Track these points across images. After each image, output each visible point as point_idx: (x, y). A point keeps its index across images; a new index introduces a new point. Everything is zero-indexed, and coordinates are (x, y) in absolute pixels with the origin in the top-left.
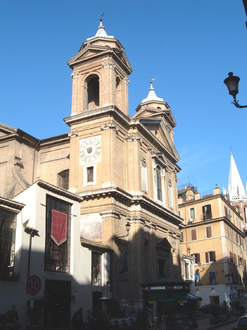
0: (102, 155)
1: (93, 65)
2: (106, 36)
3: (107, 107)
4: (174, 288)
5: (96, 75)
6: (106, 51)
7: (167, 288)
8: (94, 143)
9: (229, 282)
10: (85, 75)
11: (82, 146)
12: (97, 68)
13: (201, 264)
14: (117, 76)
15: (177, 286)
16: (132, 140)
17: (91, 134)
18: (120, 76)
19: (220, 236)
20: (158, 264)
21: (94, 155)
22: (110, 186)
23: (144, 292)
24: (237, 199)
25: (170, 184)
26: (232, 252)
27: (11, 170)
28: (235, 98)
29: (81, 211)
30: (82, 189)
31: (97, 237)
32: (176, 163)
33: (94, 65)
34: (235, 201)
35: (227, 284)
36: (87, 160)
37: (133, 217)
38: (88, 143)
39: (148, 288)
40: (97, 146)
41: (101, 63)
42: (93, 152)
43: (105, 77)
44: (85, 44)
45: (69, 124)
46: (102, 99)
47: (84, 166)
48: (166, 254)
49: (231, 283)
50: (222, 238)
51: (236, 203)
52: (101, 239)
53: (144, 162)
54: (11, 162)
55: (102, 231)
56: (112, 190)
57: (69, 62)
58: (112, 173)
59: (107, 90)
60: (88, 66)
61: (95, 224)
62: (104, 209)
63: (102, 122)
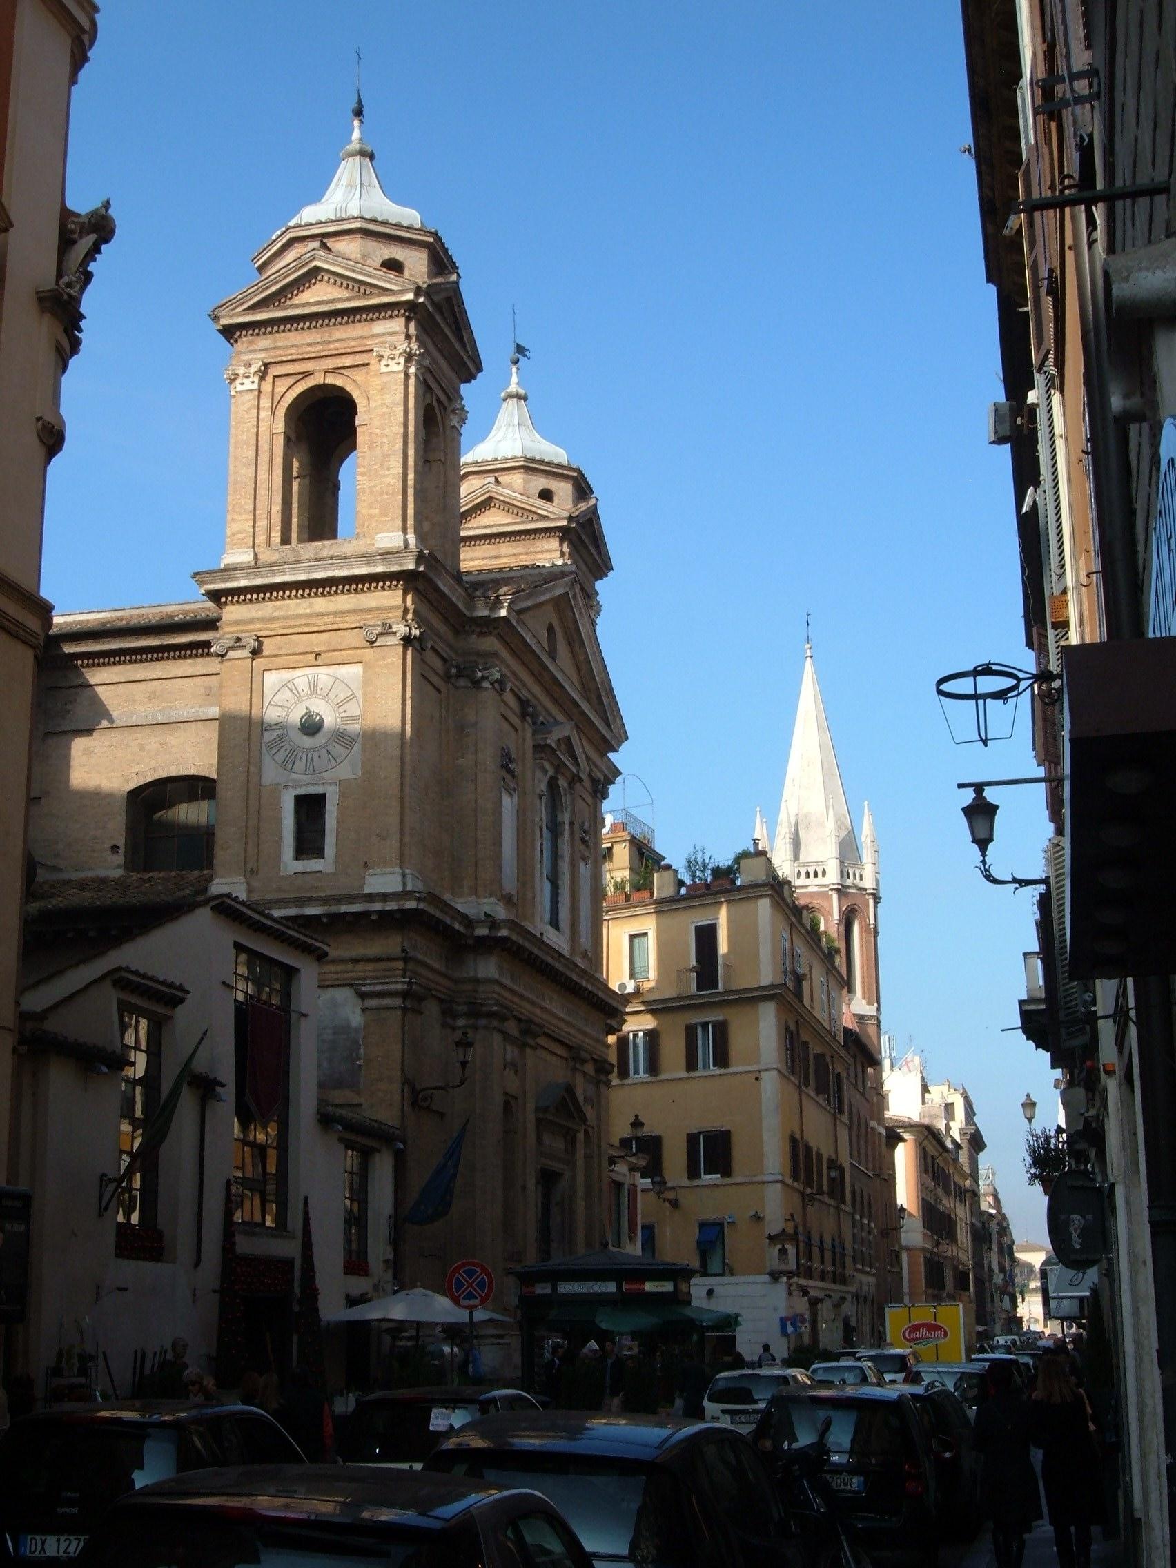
0: (364, 750)
1: (331, 346)
4: (644, 1289)
7: (619, 1287)
8: (332, 695)
9: (783, 1268)
10: (292, 380)
12: (348, 361)
15: (657, 1283)
17: (318, 654)
19: (754, 1068)
21: (330, 748)
24: (816, 875)
26: (798, 1136)
28: (984, 855)
32: (609, 755)
33: (337, 345)
34: (806, 887)
35: (775, 1276)
36: (300, 765)
38: (302, 694)
40: (341, 710)
46: (371, 507)
47: (283, 791)
49: (791, 1272)
50: (763, 1075)
51: (812, 894)
53: (509, 771)
56: (411, 905)
57: (223, 312)
59: (392, 471)
60: (309, 345)
61: (330, 1031)
62: (369, 974)
63: (369, 610)
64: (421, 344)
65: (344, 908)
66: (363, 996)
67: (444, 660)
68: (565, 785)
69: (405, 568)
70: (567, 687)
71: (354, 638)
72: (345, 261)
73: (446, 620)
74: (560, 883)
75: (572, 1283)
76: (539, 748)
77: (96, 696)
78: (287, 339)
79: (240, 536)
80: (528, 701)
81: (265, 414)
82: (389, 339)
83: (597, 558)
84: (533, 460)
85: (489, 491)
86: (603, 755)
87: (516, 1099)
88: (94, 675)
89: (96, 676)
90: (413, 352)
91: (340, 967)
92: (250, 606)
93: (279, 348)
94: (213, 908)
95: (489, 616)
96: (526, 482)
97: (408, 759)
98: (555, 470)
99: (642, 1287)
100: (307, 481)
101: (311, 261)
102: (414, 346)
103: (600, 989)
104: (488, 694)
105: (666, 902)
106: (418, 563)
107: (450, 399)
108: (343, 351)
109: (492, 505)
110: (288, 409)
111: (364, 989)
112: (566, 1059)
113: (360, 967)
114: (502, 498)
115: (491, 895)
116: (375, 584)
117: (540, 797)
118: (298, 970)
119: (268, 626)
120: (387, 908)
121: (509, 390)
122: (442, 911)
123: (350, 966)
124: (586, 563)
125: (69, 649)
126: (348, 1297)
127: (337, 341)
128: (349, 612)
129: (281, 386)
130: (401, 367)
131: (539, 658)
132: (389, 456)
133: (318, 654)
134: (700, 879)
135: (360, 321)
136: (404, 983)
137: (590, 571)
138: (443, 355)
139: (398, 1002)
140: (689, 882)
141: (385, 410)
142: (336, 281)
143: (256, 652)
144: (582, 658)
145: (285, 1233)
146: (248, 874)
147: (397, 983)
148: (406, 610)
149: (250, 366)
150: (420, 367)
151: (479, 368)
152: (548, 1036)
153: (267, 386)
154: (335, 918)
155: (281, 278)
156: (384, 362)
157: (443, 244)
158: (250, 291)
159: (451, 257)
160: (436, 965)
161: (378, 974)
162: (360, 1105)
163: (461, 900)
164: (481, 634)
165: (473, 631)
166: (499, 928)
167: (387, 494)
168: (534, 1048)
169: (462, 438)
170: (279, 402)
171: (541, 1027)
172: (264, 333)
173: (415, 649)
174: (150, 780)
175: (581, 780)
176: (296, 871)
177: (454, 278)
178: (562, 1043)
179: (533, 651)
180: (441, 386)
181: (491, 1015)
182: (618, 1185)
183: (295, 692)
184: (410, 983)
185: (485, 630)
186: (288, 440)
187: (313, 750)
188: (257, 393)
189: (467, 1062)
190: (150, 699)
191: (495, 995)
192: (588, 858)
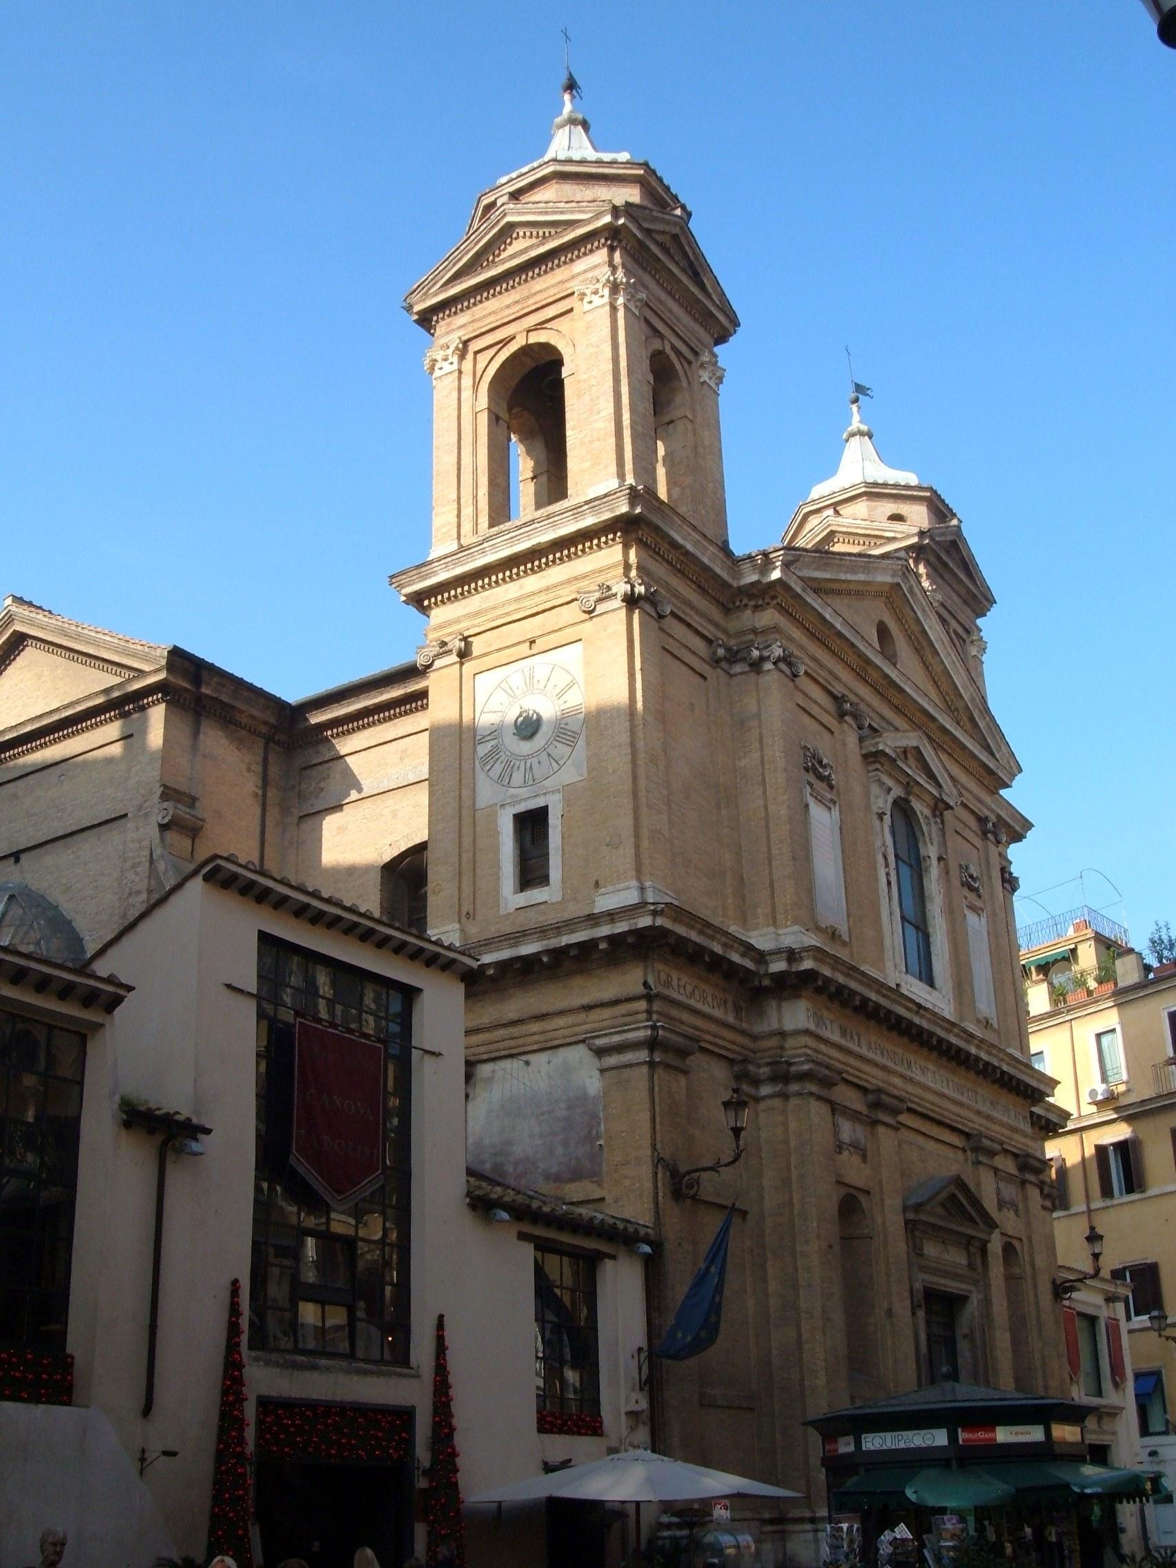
0: (588, 744)
2: (591, 155)
3: (606, 496)
5: (547, 348)
6: (588, 221)
7: (953, 1437)
8: (549, 687)
10: (492, 351)
13: (1166, 1317)
16: (751, 665)
18: (673, 348)
20: (921, 1313)
21: (551, 750)
22: (632, 897)
23: (837, 1467)
25: (972, 897)
27: (147, 853)
29: (469, 1032)
30: (379, 802)
31: (576, 1175)
33: (537, 298)
36: (518, 777)
37: (768, 1064)
38: (517, 692)
39: (851, 1439)
41: (568, 285)
44: (486, 201)
45: (420, 601)
54: (146, 814)
55: (601, 1142)
56: (645, 921)
57: (415, 298)
58: (645, 833)
59: (603, 414)
60: (508, 307)
61: (563, 1105)
64: (628, 273)
65: (565, 940)
66: (600, 1052)
67: (709, 642)
68: (927, 812)
69: (618, 513)
70: (908, 690)
71: (572, 613)
72: (536, 205)
73: (703, 590)
74: (931, 930)
75: (882, 1435)
76: (872, 758)
77: (348, 767)
78: (485, 309)
79: (444, 530)
80: (843, 696)
81: (467, 394)
82: (590, 275)
83: (970, 586)
84: (876, 484)
85: (829, 525)
86: (994, 792)
88: (344, 745)
89: (345, 746)
90: (618, 280)
91: (570, 1019)
92: (456, 604)
93: (478, 320)
94: (207, 878)
95: (758, 582)
96: (870, 510)
97: (640, 744)
98: (904, 492)
99: (991, 1435)
100: (544, 478)
101: (502, 218)
102: (620, 274)
103: (1002, 1060)
104: (771, 678)
105: (1137, 988)
106: (632, 504)
107: (968, 632)
108: (544, 303)
109: (836, 540)
110: (491, 383)
111: (600, 1042)
112: (964, 1150)
113: (595, 1015)
114: (844, 530)
115: (795, 922)
116: (589, 543)
117: (881, 816)
118: (420, 991)
120: (617, 931)
121: (850, 429)
122: (701, 932)
123: (582, 1017)
124: (959, 595)
125: (316, 718)
126: (545, 1464)
127: (535, 294)
128: (562, 583)
129: (483, 359)
130: (606, 299)
131: (853, 645)
132: (598, 398)
133: (532, 642)
134: (1167, 958)
135: (559, 266)
137: (965, 602)
138: (673, 297)
139: (643, 1055)
140: (1156, 964)
141: (591, 350)
142: (531, 233)
143: (464, 655)
144: (939, 669)
145: (406, 1371)
146: (464, 919)
147: (638, 1029)
148: (627, 567)
149: (448, 347)
150: (631, 298)
151: (735, 323)
152: (910, 1110)
153: (468, 365)
154: (559, 954)
155: (472, 245)
156: (586, 299)
157: (939, 496)
158: (441, 268)
159: (947, 506)
160: (717, 1013)
161: (617, 1022)
162: (603, 1199)
163: (755, 933)
164: (757, 608)
165: (746, 605)
166: (801, 959)
167: (599, 440)
168: (896, 1128)
169: (720, 398)
170: (482, 376)
171: (901, 1100)
172: (462, 310)
173: (643, 611)
174: (403, 849)
175: (948, 807)
176: (518, 906)
177: (955, 522)
178: (953, 1129)
179: (840, 635)
180: (677, 334)
181: (804, 1077)
182: (1092, 1320)
183: (510, 692)
184: (654, 1028)
185: (760, 602)
186: (495, 419)
187: (532, 755)
188: (456, 374)
189: (741, 1129)
190: (402, 759)
191: (809, 1051)
192: (982, 910)
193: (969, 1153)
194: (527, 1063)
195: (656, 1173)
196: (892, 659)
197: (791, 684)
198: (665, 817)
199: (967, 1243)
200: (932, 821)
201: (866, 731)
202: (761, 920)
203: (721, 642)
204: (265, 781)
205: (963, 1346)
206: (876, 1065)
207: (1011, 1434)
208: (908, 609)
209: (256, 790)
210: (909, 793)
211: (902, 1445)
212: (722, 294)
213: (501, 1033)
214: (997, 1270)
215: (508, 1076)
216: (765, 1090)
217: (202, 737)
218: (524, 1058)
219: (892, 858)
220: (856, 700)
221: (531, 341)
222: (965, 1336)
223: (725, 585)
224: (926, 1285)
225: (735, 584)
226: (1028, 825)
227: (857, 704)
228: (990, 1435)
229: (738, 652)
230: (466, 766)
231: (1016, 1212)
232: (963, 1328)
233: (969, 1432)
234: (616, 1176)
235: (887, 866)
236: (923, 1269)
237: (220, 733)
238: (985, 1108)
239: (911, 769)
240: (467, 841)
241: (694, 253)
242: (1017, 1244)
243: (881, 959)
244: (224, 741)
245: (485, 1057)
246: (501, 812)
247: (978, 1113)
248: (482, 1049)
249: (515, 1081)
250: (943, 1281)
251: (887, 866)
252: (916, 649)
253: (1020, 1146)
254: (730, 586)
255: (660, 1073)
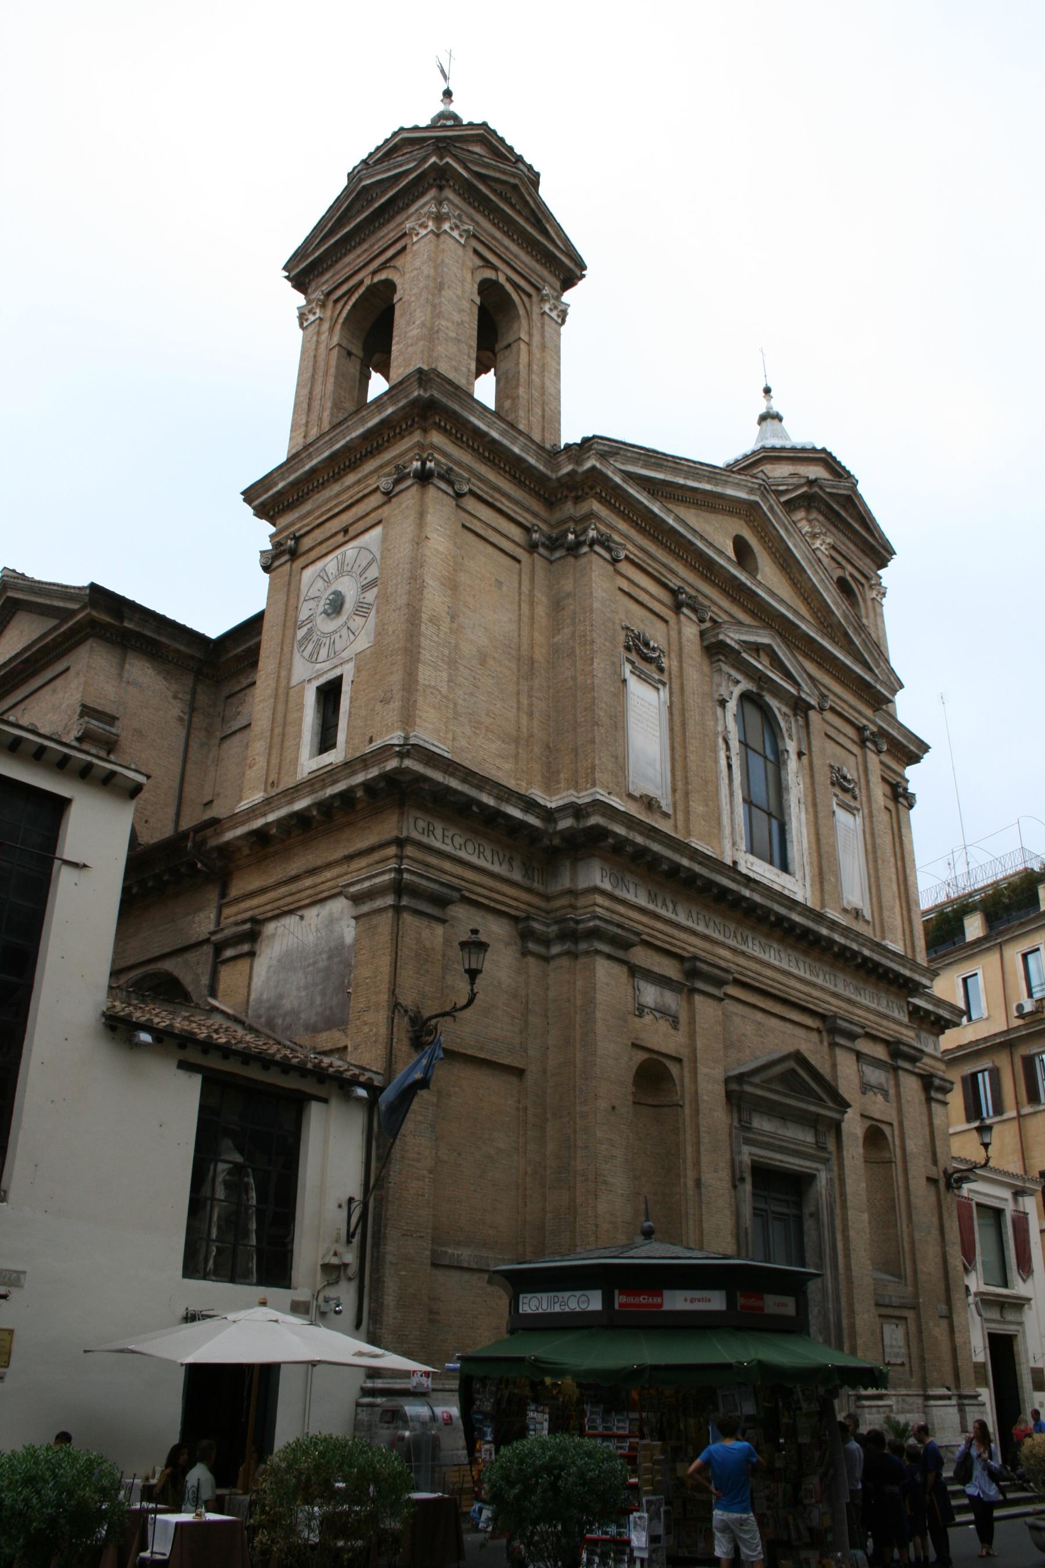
7: (608, 1301)
11: (311, 595)
14: (489, 274)
18: (509, 279)
25: (847, 798)
36: (323, 653)
42: (349, 606)
43: (415, 272)
48: (810, 1138)
52: (344, 1031)
59: (417, 323)
61: (324, 956)
66: (357, 899)
67: (527, 530)
75: (539, 1295)
87: (679, 1061)
99: (657, 1300)
112: (819, 1031)
119: (305, 522)
123: (344, 868)
136: (390, 870)
139: (389, 900)
160: (496, 868)
165: (566, 497)
166: (588, 815)
184: (399, 871)
185: (580, 493)
187: (335, 632)
193: (824, 1034)
194: (302, 917)
195: (393, 1019)
196: (752, 572)
197: (611, 568)
198: (445, 675)
199: (813, 1122)
200: (793, 720)
201: (708, 625)
202: (563, 785)
203: (536, 528)
204: (192, 709)
205: (809, 1224)
206: (694, 933)
207: (686, 1300)
208: (770, 528)
209: (181, 715)
210: (760, 688)
211: (557, 1309)
212: (566, 240)
213: (283, 890)
214: (854, 1151)
215: (287, 931)
216: (556, 950)
217: (127, 666)
218: (299, 913)
219: (735, 745)
220: (693, 593)
221: (376, 280)
222: (811, 1215)
223: (542, 478)
224: (756, 1158)
225: (554, 476)
226: (925, 748)
227: (696, 597)
228: (655, 1300)
229: (557, 539)
230: (286, 649)
231: (886, 1095)
232: (808, 1209)
233: (628, 1295)
234: (358, 1022)
235: (728, 749)
236: (748, 1142)
237: (147, 665)
238: (849, 993)
239: (762, 665)
240: (279, 716)
241: (535, 202)
242: (886, 1129)
243: (719, 837)
244: (150, 672)
245: (270, 914)
246: (307, 686)
247: (835, 995)
248: (268, 907)
249: (291, 936)
250: (778, 1156)
251: (728, 749)
252: (782, 566)
253: (892, 1033)
254: (549, 479)
255: (407, 918)
